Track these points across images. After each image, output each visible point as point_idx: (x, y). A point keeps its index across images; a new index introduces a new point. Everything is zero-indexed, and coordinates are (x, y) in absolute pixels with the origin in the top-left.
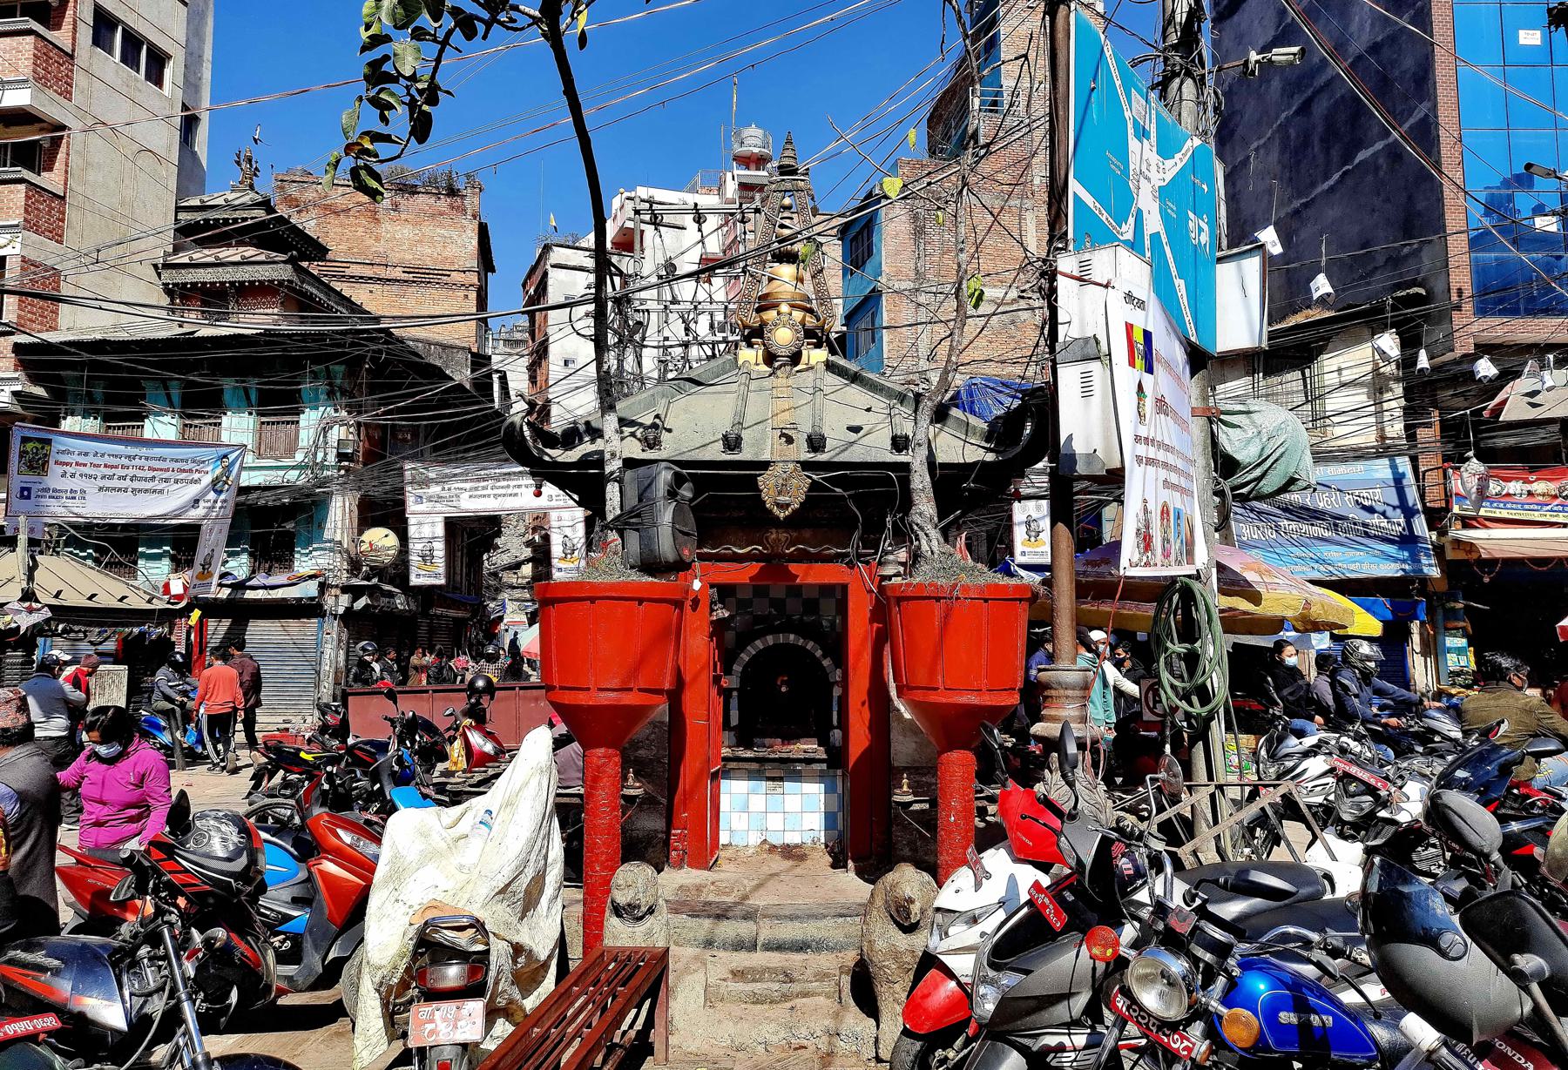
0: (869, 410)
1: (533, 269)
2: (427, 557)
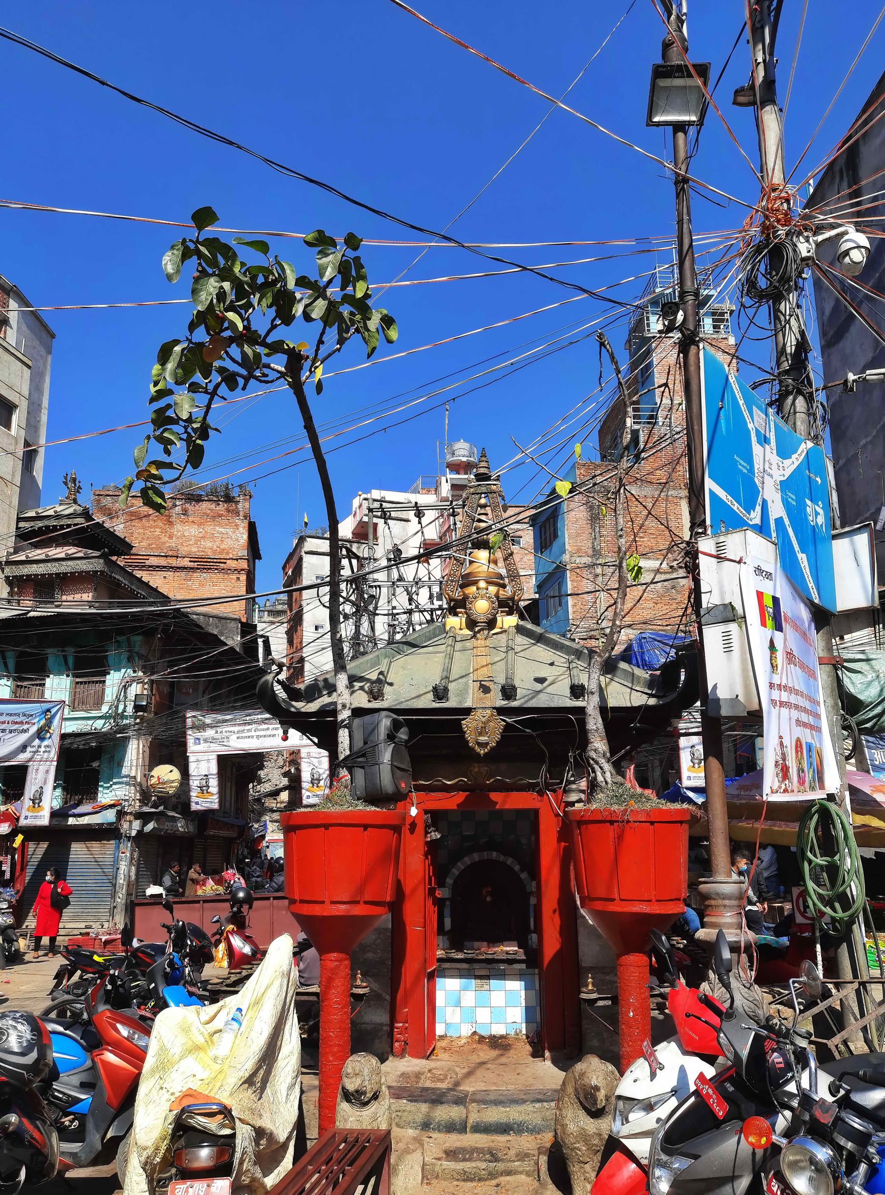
0: (552, 664)
1: (291, 555)
2: (204, 789)
